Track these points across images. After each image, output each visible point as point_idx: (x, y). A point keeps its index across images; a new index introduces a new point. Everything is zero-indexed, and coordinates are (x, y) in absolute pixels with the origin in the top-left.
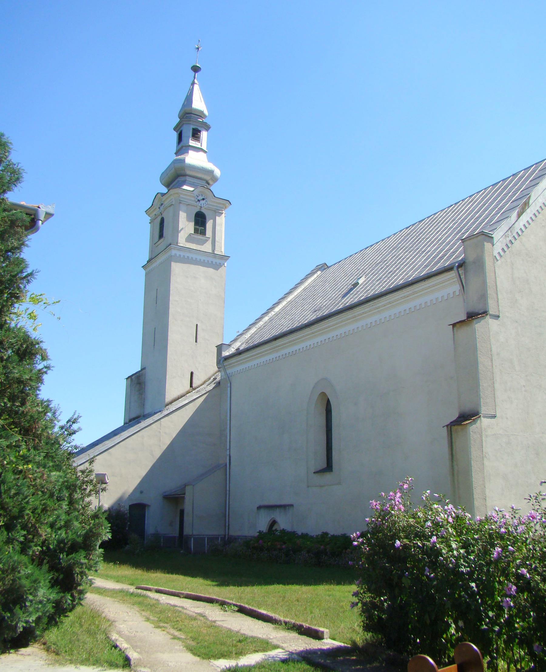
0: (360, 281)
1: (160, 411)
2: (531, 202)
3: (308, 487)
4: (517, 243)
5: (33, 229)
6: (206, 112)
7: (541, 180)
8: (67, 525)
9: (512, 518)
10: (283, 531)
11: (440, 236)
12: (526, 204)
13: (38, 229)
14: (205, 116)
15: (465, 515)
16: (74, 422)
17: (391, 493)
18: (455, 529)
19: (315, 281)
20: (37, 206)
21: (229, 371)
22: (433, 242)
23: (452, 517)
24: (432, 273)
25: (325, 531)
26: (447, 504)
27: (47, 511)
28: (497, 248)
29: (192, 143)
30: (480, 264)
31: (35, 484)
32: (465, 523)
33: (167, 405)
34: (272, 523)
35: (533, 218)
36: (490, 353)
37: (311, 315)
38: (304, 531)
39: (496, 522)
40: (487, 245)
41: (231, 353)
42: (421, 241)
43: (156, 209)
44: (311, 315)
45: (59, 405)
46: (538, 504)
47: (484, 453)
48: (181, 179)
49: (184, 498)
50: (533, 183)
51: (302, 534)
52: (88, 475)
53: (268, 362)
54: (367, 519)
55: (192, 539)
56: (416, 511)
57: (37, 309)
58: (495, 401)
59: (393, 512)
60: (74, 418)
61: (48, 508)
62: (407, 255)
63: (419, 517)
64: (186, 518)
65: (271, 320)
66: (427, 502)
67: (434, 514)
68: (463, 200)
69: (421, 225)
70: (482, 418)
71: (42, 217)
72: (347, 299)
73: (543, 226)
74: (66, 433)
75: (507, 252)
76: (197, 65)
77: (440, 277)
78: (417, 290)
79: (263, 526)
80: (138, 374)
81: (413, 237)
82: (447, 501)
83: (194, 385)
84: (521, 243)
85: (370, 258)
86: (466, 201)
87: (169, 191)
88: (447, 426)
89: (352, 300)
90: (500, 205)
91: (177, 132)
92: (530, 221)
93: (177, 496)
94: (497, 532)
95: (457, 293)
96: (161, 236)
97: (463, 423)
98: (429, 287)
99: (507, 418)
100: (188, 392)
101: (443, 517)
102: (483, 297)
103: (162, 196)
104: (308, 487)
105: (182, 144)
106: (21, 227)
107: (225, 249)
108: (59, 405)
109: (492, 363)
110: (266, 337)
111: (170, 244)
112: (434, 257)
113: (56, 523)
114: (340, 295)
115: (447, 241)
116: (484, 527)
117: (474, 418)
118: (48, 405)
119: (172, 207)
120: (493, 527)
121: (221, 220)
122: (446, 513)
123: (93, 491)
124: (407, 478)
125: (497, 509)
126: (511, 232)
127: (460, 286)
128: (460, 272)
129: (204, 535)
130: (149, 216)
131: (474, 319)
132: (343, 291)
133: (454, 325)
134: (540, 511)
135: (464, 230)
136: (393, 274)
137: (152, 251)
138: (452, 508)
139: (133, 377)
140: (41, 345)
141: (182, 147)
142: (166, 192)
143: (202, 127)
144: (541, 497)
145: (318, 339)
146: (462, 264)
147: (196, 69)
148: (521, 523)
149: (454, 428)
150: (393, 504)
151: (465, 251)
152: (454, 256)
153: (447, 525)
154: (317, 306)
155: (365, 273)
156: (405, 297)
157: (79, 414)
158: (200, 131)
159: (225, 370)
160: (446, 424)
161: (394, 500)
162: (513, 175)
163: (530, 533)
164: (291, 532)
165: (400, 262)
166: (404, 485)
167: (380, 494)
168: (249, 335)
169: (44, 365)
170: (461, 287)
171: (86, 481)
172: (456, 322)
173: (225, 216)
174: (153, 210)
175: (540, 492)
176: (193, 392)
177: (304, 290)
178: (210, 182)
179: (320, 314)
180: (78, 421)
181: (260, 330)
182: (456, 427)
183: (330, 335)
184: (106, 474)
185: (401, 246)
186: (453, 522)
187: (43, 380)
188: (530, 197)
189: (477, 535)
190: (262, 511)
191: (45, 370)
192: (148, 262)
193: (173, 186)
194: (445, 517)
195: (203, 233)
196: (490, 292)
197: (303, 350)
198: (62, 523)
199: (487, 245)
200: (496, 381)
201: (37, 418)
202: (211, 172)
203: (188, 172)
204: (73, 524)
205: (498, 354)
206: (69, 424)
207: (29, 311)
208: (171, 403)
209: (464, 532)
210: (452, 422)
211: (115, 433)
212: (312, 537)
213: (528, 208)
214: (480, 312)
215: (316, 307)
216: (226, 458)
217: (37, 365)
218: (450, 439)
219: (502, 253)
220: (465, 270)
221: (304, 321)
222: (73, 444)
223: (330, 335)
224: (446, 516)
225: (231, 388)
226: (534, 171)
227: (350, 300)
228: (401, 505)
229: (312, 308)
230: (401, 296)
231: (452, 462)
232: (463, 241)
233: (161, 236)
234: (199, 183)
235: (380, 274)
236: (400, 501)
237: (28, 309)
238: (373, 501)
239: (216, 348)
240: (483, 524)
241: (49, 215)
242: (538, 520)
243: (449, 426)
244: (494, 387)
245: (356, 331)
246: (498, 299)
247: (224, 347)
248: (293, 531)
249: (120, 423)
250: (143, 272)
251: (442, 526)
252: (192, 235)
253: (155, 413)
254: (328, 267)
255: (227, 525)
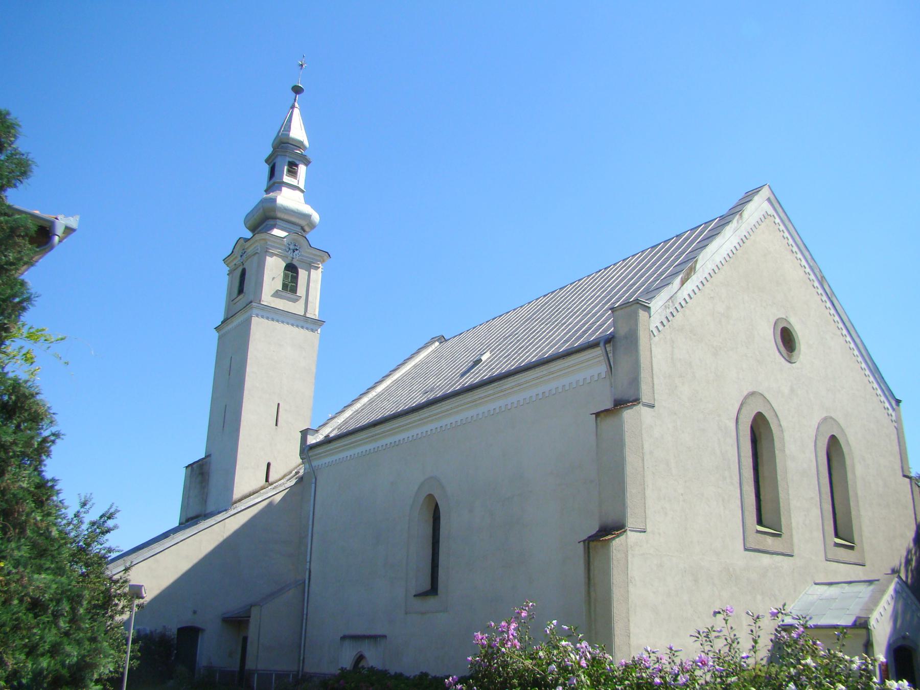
0: (484, 358)
1: (226, 510)
2: (698, 266)
3: (406, 613)
4: (679, 316)
5: (46, 246)
6: (306, 143)
7: (711, 242)
8: (55, 650)
9: (669, 663)
10: (371, 669)
11: (585, 307)
12: (692, 269)
13: (52, 248)
14: (305, 148)
15: (604, 658)
16: (109, 518)
17: (503, 623)
18: (590, 676)
19: (428, 357)
20: (55, 217)
21: (315, 463)
22: (576, 313)
23: (586, 659)
24: (573, 349)
25: (424, 672)
26: (580, 640)
27: (20, 629)
28: (655, 322)
29: (287, 179)
30: (632, 339)
31: (8, 590)
32: (603, 669)
33: (236, 502)
34: (358, 659)
35: (701, 286)
36: (641, 451)
37: (421, 397)
38: (399, 670)
39: (647, 668)
40: (642, 314)
41: (318, 440)
42: (561, 312)
43: (236, 257)
44: (421, 397)
45: (91, 494)
46: (709, 643)
47: (629, 578)
48: (271, 222)
49: (248, 621)
50: (701, 245)
51: (396, 673)
52: (122, 586)
53: (364, 453)
54: (470, 658)
55: (256, 675)
56: (537, 649)
57: (37, 350)
58: (645, 511)
59: (503, 649)
60: (110, 512)
61: (22, 625)
62: (543, 328)
63: (540, 657)
64: (249, 648)
65: (371, 402)
66: (552, 636)
67: (561, 655)
68: (615, 265)
69: (562, 293)
70: (628, 532)
71: (59, 230)
72: (466, 378)
73: (711, 297)
74: (98, 530)
75: (667, 327)
76: (300, 85)
77: (583, 355)
78: (552, 369)
79: (346, 660)
80: (200, 462)
81: (551, 308)
82: (581, 635)
83: (271, 480)
84: (684, 316)
85: (498, 331)
86: (618, 265)
87: (254, 235)
88: (584, 541)
89: (472, 379)
90: (660, 270)
91: (269, 165)
92: (696, 290)
93: (239, 619)
94: (648, 682)
95: (603, 375)
96: (241, 291)
97: (601, 539)
98: (569, 367)
99: (659, 534)
100: (263, 488)
101: (574, 659)
102: (635, 381)
103: (245, 242)
104: (406, 613)
105: (274, 180)
106: (23, 237)
107: (319, 312)
108: (91, 494)
109: (643, 464)
110: (365, 422)
111: (251, 302)
112: (577, 331)
113: (38, 647)
114: (458, 373)
115: (593, 312)
116: (631, 674)
117: (618, 532)
118: (53, 487)
119: (257, 255)
120: (644, 675)
121: (317, 275)
122: (577, 654)
123: (127, 607)
124: (527, 602)
125: (649, 649)
126: (672, 302)
127: (607, 366)
128: (608, 349)
129: (270, 671)
130: (228, 266)
131: (623, 407)
132: (463, 369)
133: (597, 414)
134: (711, 654)
135: (614, 299)
136: (525, 349)
137: (228, 309)
138: (586, 647)
139: (194, 466)
140: (39, 397)
141: (274, 183)
142: (249, 238)
143: (299, 160)
144: (714, 634)
145: (428, 427)
146: (609, 340)
147: (297, 90)
148: (683, 670)
149: (592, 544)
150: (505, 639)
151: (614, 324)
152: (601, 330)
153: (579, 670)
154: (429, 387)
155: (490, 348)
156: (538, 378)
157: (117, 507)
158: (297, 166)
159: (310, 462)
160: (582, 539)
161: (507, 633)
162: (677, 236)
163: (696, 684)
164: (381, 671)
165: (534, 336)
166: (522, 612)
167: (489, 623)
168: (343, 420)
169: (51, 431)
170: (608, 367)
171: (119, 594)
172: (599, 410)
173: (322, 272)
174: (231, 259)
175: (712, 627)
176: (270, 488)
177: (415, 367)
178: (307, 229)
179: (431, 396)
180: (116, 516)
181: (357, 414)
182: (595, 543)
183: (443, 422)
184: (142, 586)
185: (536, 317)
186: (588, 666)
187: (51, 451)
188: (697, 260)
189: (620, 685)
190: (347, 643)
191: (53, 438)
192: (223, 322)
193: (260, 230)
194: (576, 659)
195: (294, 290)
196: (644, 375)
197: (408, 440)
198: (47, 647)
199: (642, 314)
200: (648, 486)
201: (21, 499)
202: (307, 217)
203: (279, 215)
204: (64, 648)
205: (651, 453)
206: (102, 520)
207: (24, 351)
208: (240, 500)
209: (603, 681)
210: (590, 537)
211: (166, 535)
212: (408, 678)
213: (694, 274)
214: (631, 400)
215: (428, 388)
216: (305, 574)
217: (42, 431)
218: (586, 555)
219: (661, 328)
220: (614, 346)
221: (412, 404)
222: (107, 545)
223: (443, 422)
224: (578, 657)
225: (316, 484)
226: (702, 232)
227: (469, 380)
228: (516, 640)
229: (423, 388)
230: (532, 377)
231: (589, 587)
232: (612, 309)
233: (241, 291)
234: (292, 228)
235: (508, 350)
236: (515, 634)
237: (22, 348)
238: (479, 633)
239: (300, 434)
240: (629, 670)
241: (69, 230)
242: (709, 666)
243: (587, 542)
244: (644, 493)
245: (475, 418)
246: (653, 384)
247: (310, 432)
248: (384, 669)
249: (176, 524)
250: (216, 335)
251: (572, 672)
252: (279, 293)
253: (219, 513)
254: (446, 341)
255: (302, 658)
